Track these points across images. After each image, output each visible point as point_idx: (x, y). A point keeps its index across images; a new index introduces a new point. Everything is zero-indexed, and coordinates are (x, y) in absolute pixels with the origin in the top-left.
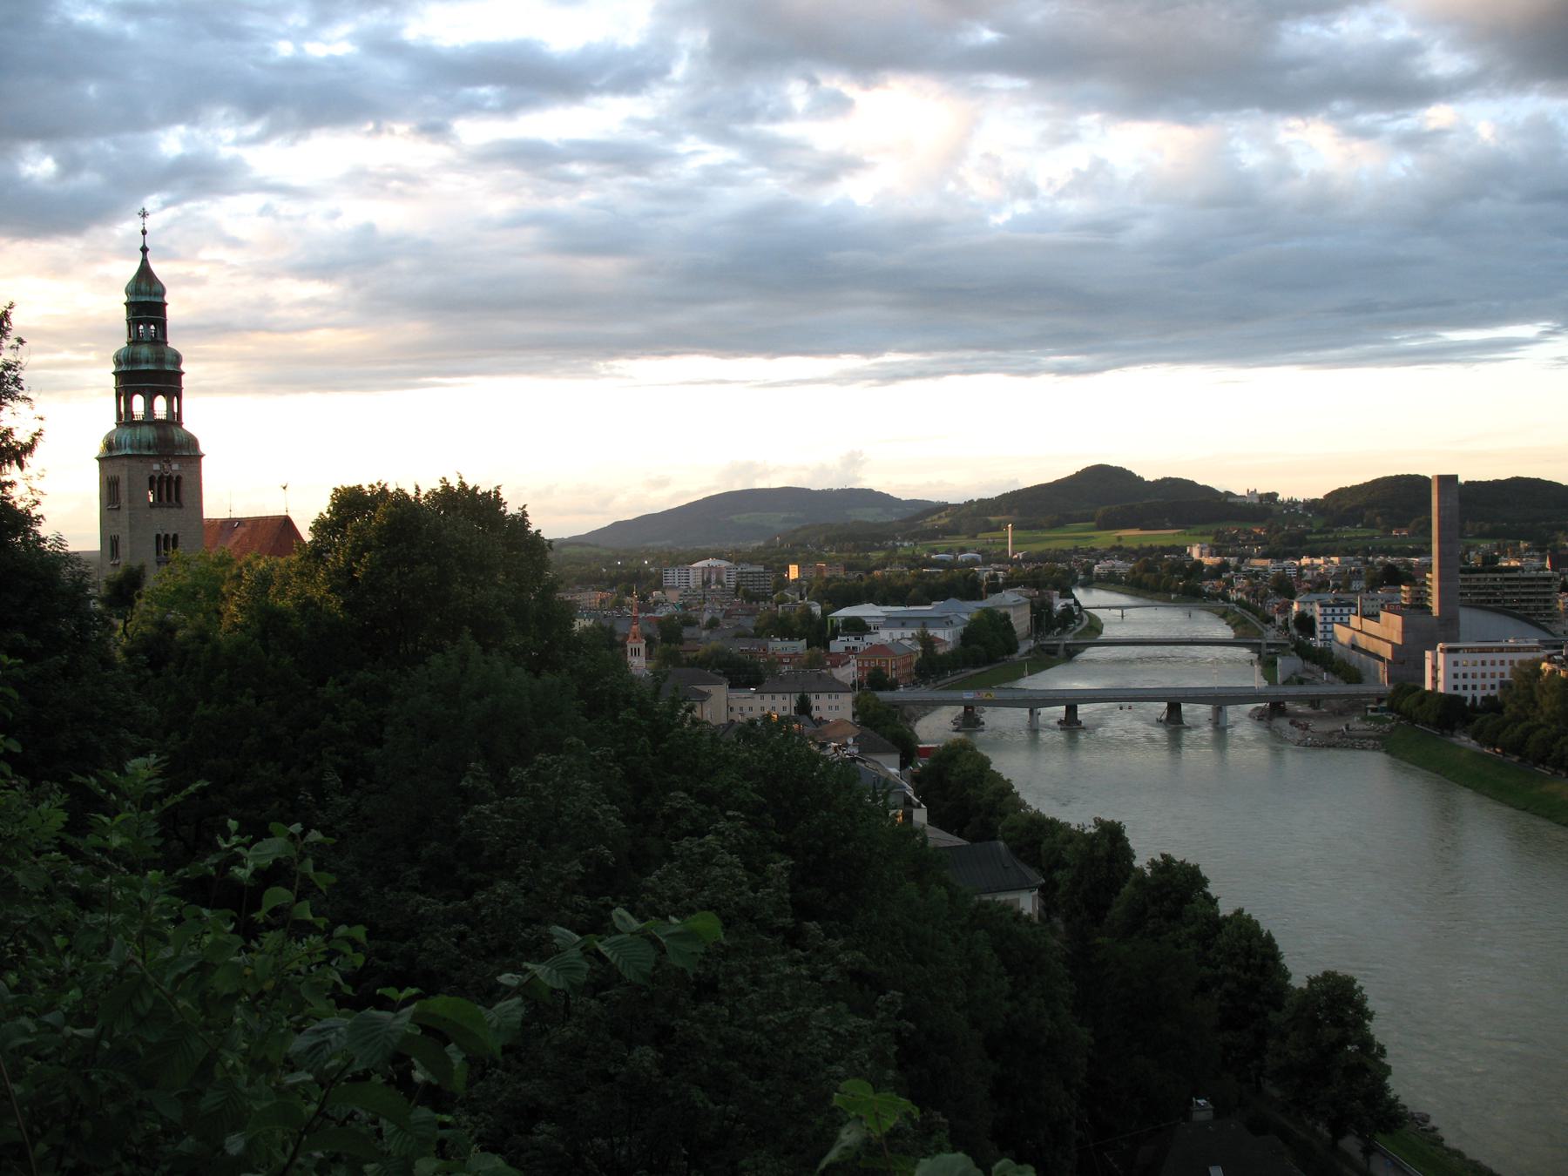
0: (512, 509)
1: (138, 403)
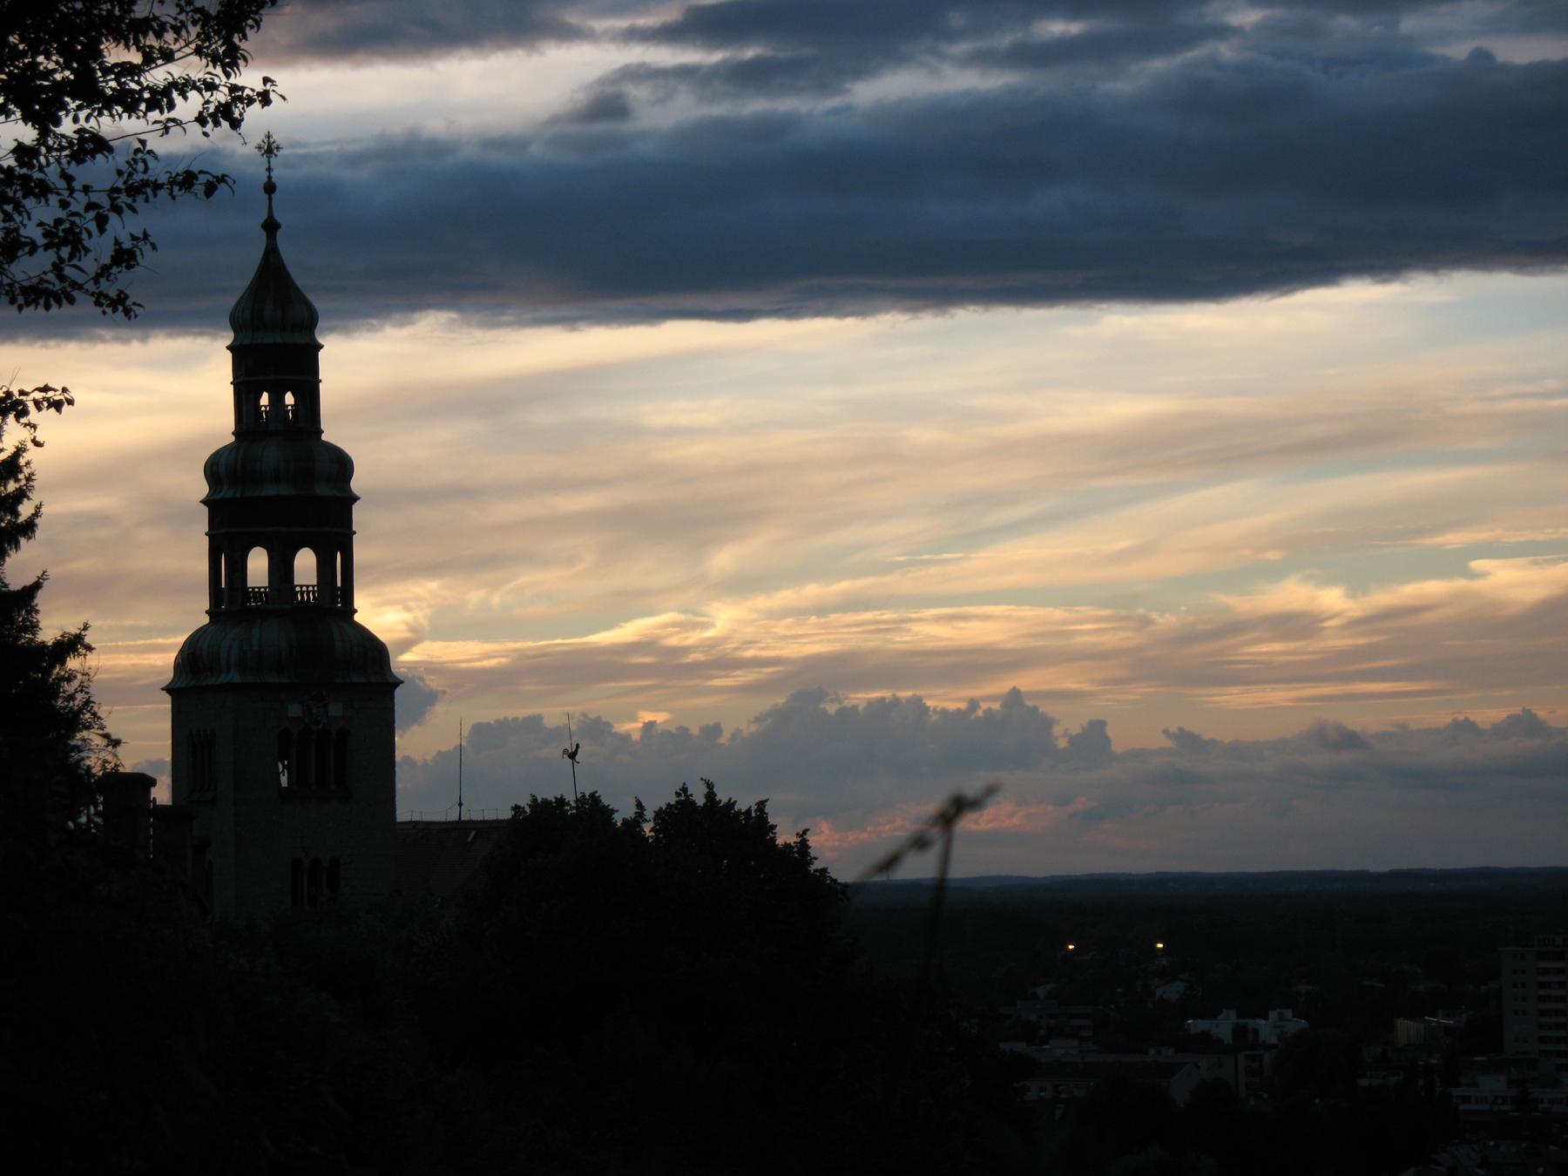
0: (785, 836)
1: (258, 564)
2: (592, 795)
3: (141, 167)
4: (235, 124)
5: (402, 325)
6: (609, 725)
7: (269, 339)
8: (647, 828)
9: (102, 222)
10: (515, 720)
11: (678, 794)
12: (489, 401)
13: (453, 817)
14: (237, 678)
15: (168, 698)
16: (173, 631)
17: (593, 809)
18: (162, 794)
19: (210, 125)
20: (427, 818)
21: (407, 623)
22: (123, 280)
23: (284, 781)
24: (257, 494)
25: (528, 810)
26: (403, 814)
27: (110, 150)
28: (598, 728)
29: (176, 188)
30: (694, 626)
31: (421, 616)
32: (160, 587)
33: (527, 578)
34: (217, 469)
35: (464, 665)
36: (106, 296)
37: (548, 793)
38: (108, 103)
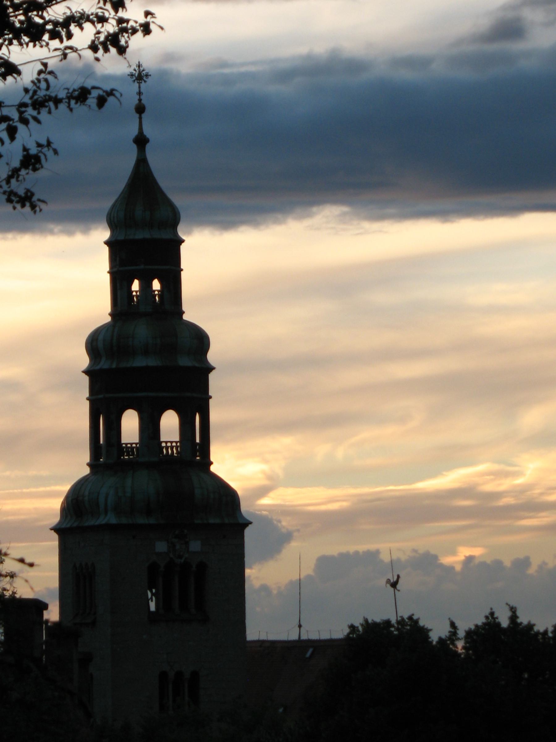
1: (130, 424)
2: (410, 618)
3: (43, 85)
4: (122, 50)
5: (301, 218)
6: (435, 557)
7: (140, 235)
8: (460, 645)
9: (12, 132)
10: (357, 553)
11: (487, 617)
12: (340, 285)
13: (294, 637)
14: (112, 519)
15: (56, 536)
16: (61, 480)
17: (412, 632)
18: (53, 614)
19: (101, 51)
20: (272, 637)
21: (264, 472)
22: (29, 179)
23: (153, 606)
24: (129, 365)
25: (360, 629)
26: (253, 633)
27: (19, 73)
28: (427, 561)
29: (73, 102)
30: (507, 475)
31: (277, 467)
32: (54, 443)
33: (367, 434)
34: (97, 344)
35: (311, 508)
36: (16, 194)
37: (376, 617)
38: (17, 34)
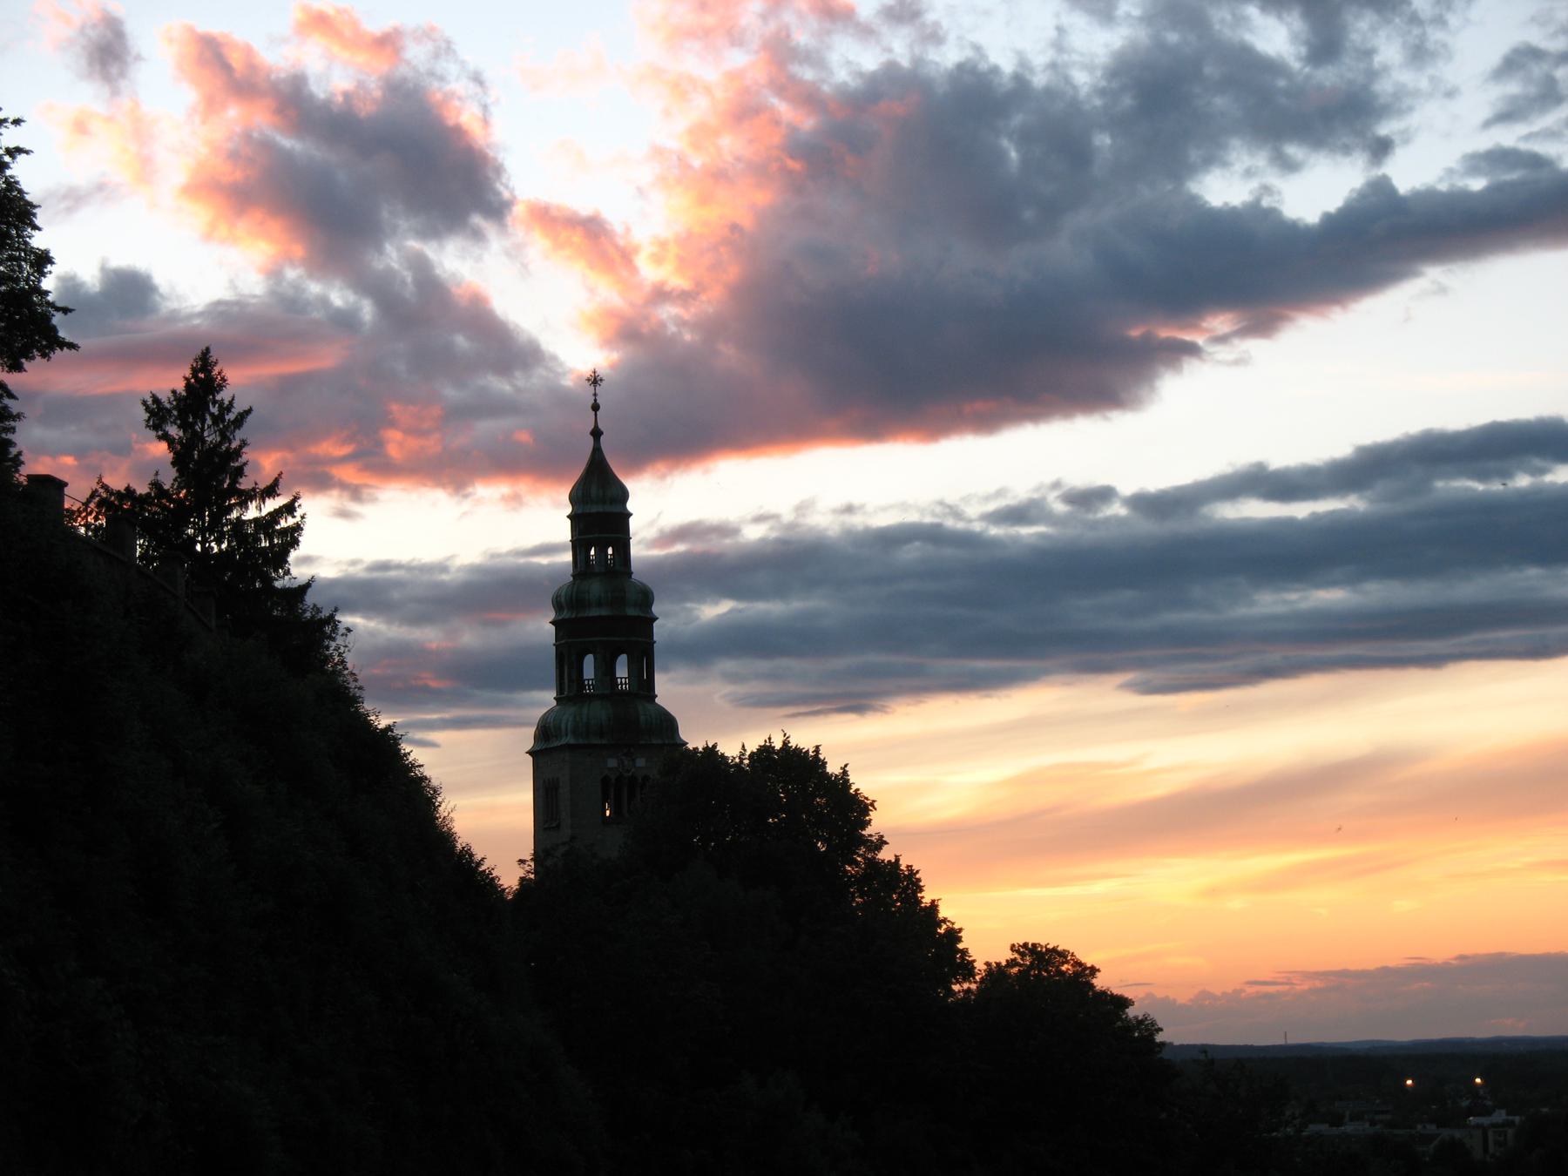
7: (594, 509)
14: (570, 740)
